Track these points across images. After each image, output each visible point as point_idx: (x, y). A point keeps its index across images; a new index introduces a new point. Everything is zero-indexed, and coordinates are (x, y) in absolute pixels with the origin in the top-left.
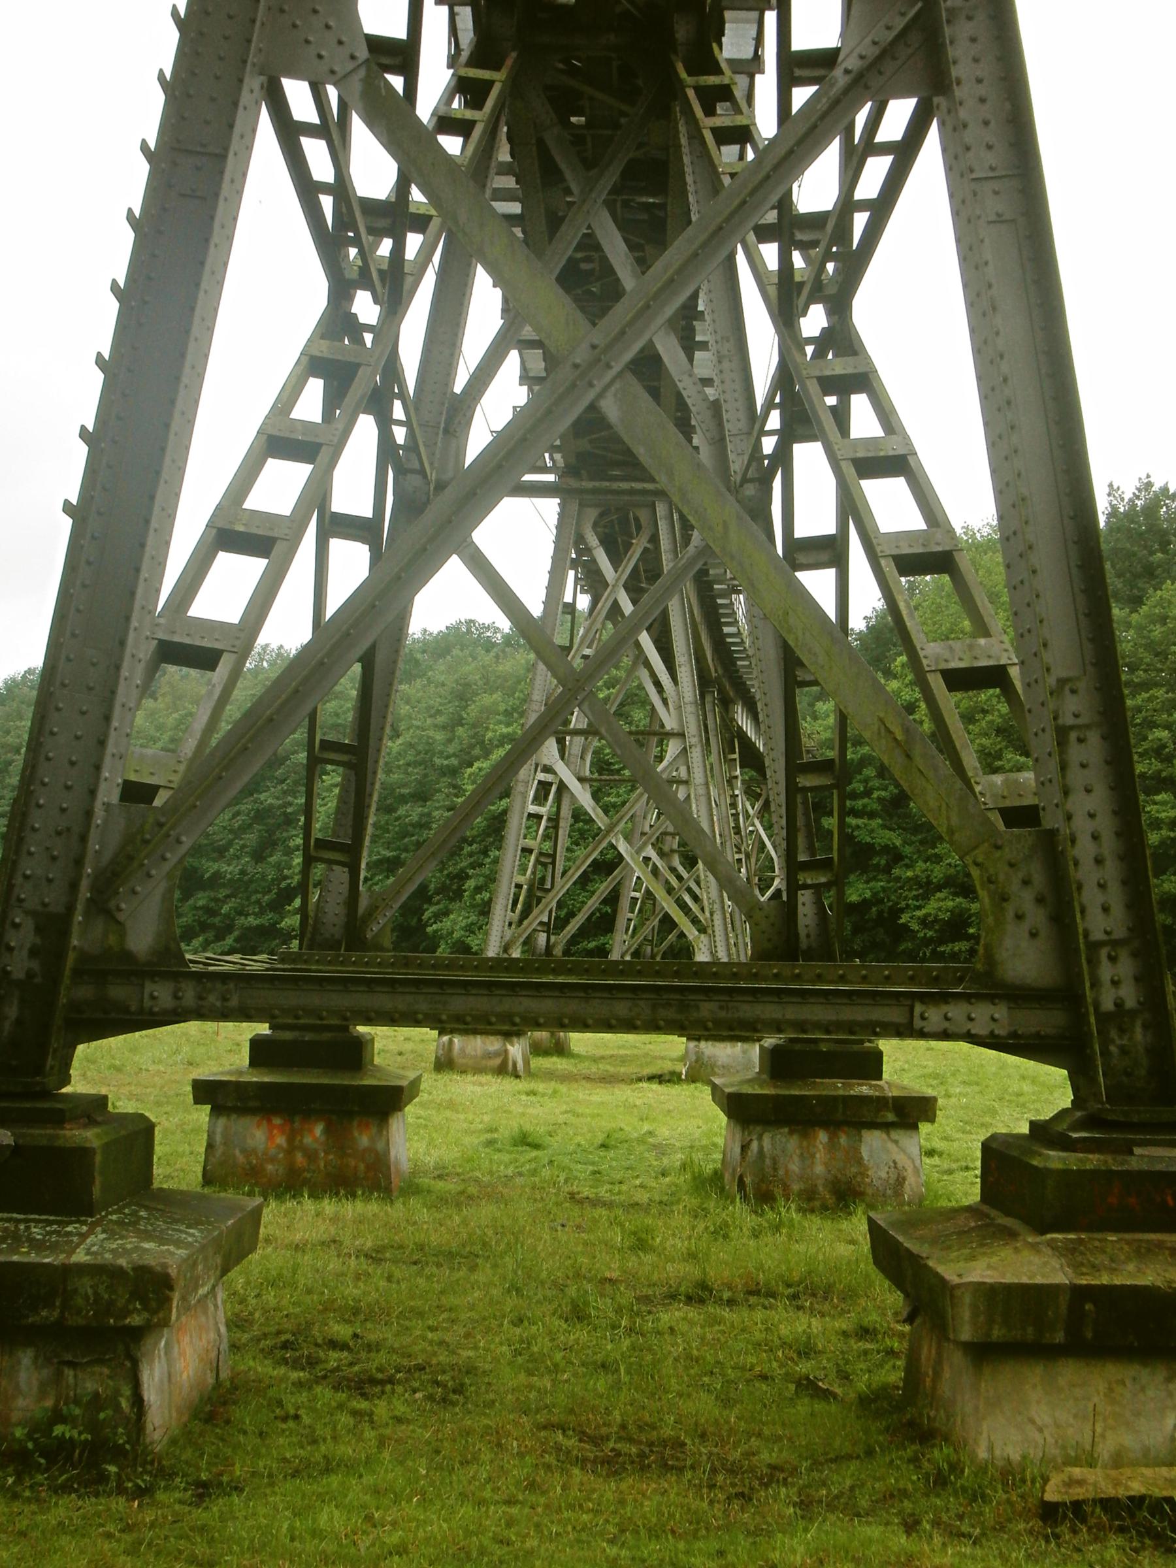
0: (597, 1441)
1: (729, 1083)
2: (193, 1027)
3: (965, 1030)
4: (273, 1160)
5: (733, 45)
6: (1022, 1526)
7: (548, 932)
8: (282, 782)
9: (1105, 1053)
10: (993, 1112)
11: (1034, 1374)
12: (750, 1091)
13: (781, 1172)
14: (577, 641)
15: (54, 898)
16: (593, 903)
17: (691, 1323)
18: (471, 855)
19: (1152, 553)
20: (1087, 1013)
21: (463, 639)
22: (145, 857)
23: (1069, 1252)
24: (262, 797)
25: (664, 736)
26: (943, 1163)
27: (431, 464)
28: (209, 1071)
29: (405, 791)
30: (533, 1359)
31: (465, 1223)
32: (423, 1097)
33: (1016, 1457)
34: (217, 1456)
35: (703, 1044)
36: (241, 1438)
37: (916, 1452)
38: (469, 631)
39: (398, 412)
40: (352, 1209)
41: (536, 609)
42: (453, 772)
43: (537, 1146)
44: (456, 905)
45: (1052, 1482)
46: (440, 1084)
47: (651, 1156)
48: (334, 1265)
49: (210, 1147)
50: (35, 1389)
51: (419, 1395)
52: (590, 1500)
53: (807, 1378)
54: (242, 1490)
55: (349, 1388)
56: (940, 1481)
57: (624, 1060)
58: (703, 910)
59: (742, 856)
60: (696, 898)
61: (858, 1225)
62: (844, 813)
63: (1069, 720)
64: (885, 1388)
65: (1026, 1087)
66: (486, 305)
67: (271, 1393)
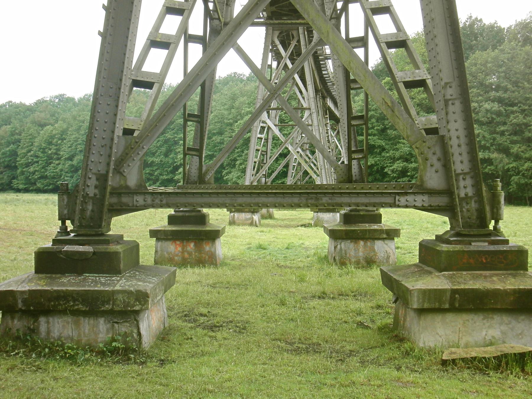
0: (292, 344)
1: (330, 226)
2: (152, 210)
3: (413, 205)
4: (177, 255)
6: (435, 368)
7: (265, 177)
8: (173, 130)
9: (462, 211)
10: (419, 234)
11: (438, 318)
12: (337, 228)
13: (348, 255)
14: (273, 78)
15: (102, 168)
16: (280, 168)
17: (321, 305)
18: (238, 152)
19: (472, 41)
20: (455, 198)
21: (233, 79)
22: (133, 153)
23: (450, 278)
24: (166, 135)
25: (303, 109)
26: (405, 250)
27: (222, 16)
28: (154, 227)
29: (215, 131)
30: (268, 318)
31: (242, 274)
32: (226, 234)
33: (432, 345)
34: (166, 351)
35: (319, 214)
36: (174, 346)
37: (399, 345)
38: (235, 76)
40: (205, 271)
41: (259, 66)
42: (231, 125)
43: (265, 249)
44: (233, 170)
45: (445, 353)
46: (231, 229)
47: (303, 251)
48: (200, 289)
49: (156, 252)
50: (105, 331)
51: (231, 330)
52: (290, 363)
53: (360, 322)
54: (175, 362)
55: (208, 329)
56: (407, 354)
57: (292, 220)
58: (318, 169)
59: (330, 150)
60: (315, 165)
61: (376, 272)
62: (368, 135)
63: (449, 97)
64: (386, 324)
65: (429, 226)
67: (182, 331)
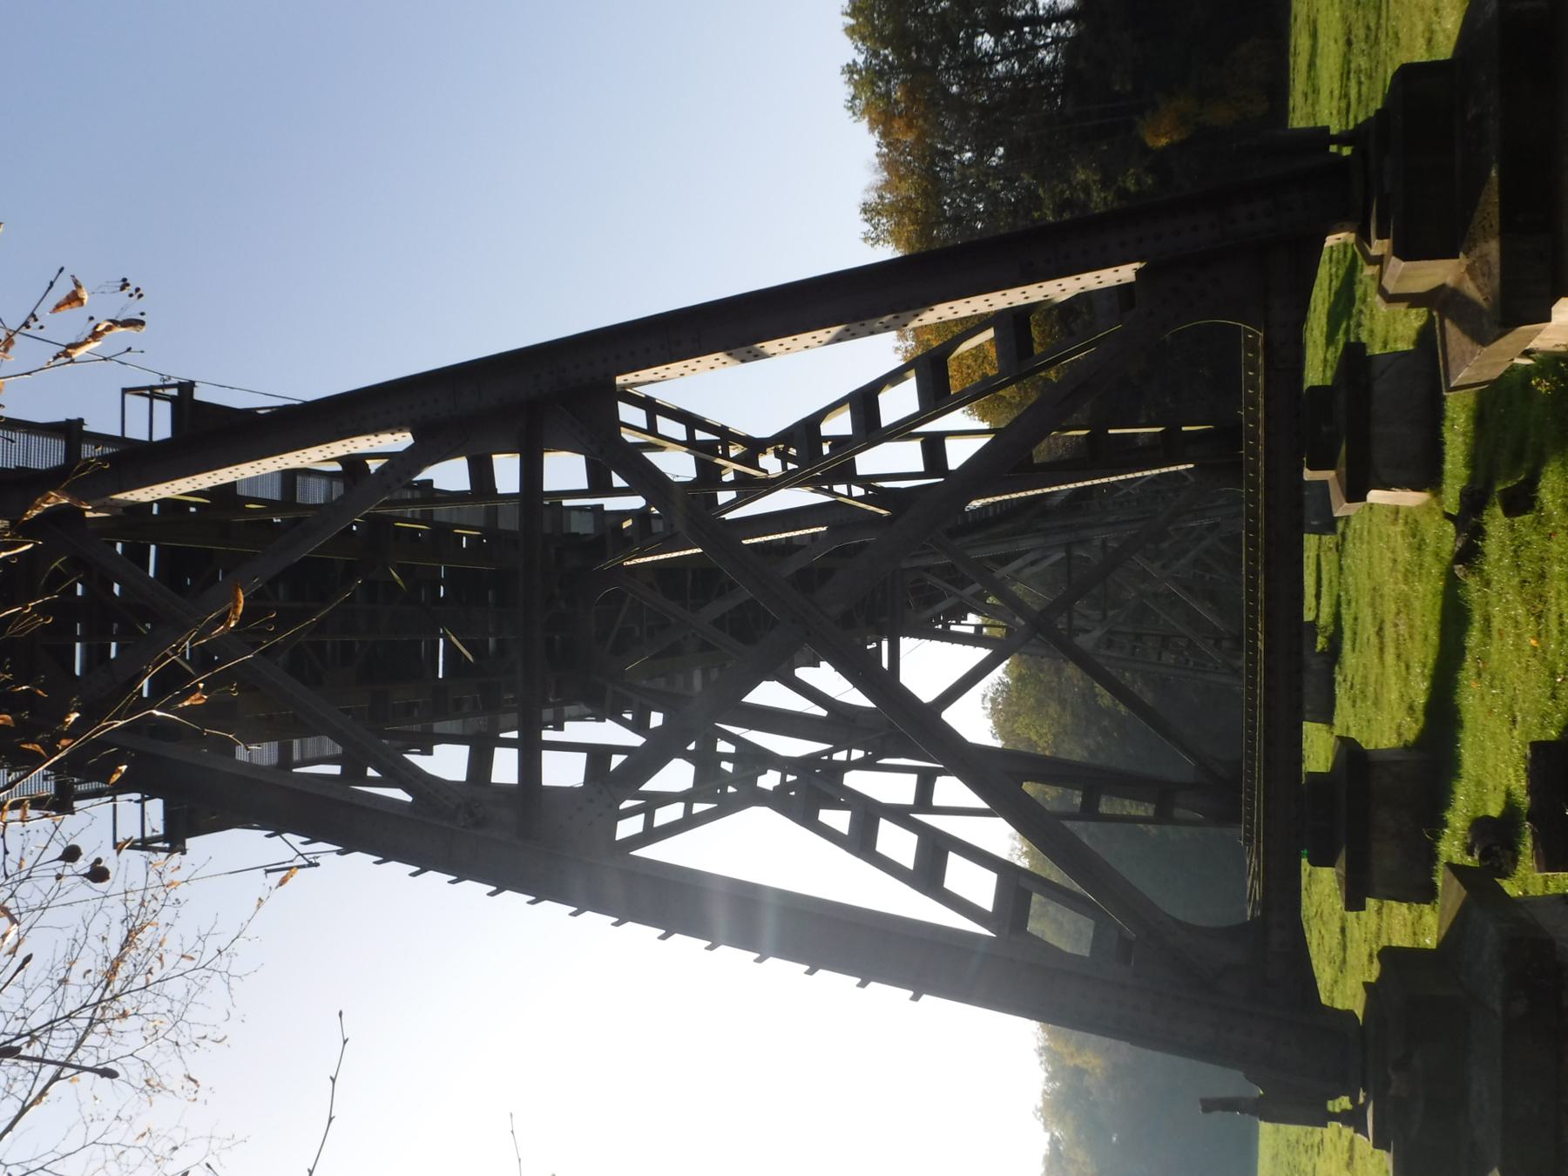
5: (582, 526)
21: (1004, 711)
39: (840, 756)
41: (981, 653)
66: (769, 694)
